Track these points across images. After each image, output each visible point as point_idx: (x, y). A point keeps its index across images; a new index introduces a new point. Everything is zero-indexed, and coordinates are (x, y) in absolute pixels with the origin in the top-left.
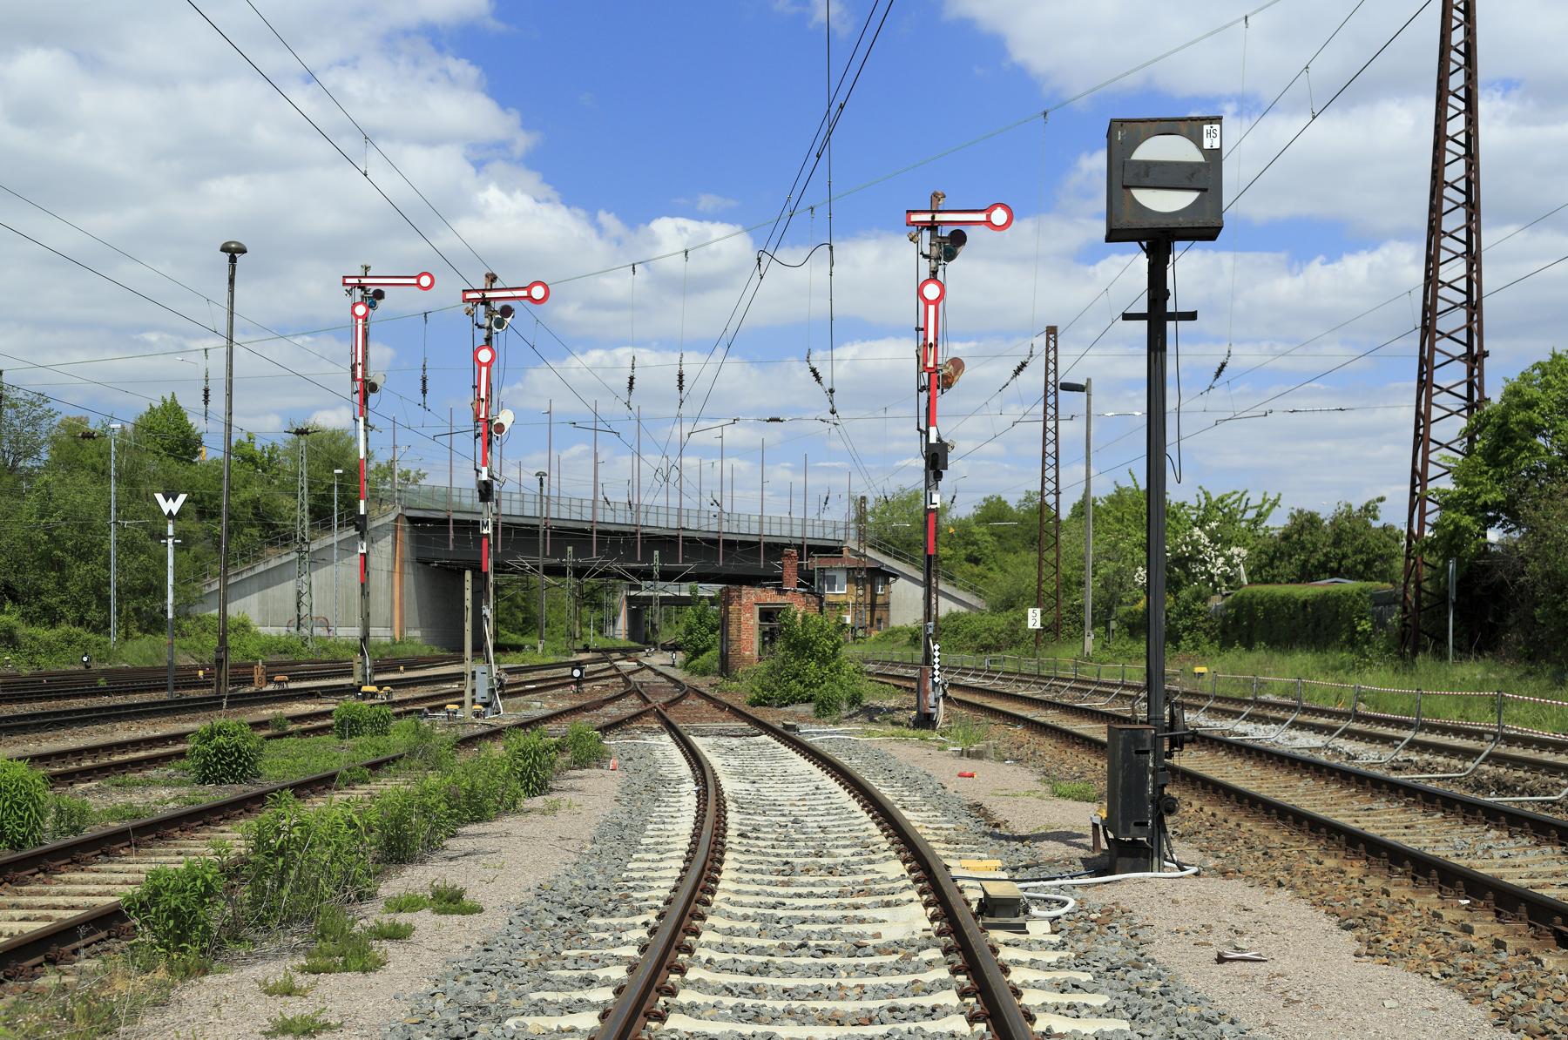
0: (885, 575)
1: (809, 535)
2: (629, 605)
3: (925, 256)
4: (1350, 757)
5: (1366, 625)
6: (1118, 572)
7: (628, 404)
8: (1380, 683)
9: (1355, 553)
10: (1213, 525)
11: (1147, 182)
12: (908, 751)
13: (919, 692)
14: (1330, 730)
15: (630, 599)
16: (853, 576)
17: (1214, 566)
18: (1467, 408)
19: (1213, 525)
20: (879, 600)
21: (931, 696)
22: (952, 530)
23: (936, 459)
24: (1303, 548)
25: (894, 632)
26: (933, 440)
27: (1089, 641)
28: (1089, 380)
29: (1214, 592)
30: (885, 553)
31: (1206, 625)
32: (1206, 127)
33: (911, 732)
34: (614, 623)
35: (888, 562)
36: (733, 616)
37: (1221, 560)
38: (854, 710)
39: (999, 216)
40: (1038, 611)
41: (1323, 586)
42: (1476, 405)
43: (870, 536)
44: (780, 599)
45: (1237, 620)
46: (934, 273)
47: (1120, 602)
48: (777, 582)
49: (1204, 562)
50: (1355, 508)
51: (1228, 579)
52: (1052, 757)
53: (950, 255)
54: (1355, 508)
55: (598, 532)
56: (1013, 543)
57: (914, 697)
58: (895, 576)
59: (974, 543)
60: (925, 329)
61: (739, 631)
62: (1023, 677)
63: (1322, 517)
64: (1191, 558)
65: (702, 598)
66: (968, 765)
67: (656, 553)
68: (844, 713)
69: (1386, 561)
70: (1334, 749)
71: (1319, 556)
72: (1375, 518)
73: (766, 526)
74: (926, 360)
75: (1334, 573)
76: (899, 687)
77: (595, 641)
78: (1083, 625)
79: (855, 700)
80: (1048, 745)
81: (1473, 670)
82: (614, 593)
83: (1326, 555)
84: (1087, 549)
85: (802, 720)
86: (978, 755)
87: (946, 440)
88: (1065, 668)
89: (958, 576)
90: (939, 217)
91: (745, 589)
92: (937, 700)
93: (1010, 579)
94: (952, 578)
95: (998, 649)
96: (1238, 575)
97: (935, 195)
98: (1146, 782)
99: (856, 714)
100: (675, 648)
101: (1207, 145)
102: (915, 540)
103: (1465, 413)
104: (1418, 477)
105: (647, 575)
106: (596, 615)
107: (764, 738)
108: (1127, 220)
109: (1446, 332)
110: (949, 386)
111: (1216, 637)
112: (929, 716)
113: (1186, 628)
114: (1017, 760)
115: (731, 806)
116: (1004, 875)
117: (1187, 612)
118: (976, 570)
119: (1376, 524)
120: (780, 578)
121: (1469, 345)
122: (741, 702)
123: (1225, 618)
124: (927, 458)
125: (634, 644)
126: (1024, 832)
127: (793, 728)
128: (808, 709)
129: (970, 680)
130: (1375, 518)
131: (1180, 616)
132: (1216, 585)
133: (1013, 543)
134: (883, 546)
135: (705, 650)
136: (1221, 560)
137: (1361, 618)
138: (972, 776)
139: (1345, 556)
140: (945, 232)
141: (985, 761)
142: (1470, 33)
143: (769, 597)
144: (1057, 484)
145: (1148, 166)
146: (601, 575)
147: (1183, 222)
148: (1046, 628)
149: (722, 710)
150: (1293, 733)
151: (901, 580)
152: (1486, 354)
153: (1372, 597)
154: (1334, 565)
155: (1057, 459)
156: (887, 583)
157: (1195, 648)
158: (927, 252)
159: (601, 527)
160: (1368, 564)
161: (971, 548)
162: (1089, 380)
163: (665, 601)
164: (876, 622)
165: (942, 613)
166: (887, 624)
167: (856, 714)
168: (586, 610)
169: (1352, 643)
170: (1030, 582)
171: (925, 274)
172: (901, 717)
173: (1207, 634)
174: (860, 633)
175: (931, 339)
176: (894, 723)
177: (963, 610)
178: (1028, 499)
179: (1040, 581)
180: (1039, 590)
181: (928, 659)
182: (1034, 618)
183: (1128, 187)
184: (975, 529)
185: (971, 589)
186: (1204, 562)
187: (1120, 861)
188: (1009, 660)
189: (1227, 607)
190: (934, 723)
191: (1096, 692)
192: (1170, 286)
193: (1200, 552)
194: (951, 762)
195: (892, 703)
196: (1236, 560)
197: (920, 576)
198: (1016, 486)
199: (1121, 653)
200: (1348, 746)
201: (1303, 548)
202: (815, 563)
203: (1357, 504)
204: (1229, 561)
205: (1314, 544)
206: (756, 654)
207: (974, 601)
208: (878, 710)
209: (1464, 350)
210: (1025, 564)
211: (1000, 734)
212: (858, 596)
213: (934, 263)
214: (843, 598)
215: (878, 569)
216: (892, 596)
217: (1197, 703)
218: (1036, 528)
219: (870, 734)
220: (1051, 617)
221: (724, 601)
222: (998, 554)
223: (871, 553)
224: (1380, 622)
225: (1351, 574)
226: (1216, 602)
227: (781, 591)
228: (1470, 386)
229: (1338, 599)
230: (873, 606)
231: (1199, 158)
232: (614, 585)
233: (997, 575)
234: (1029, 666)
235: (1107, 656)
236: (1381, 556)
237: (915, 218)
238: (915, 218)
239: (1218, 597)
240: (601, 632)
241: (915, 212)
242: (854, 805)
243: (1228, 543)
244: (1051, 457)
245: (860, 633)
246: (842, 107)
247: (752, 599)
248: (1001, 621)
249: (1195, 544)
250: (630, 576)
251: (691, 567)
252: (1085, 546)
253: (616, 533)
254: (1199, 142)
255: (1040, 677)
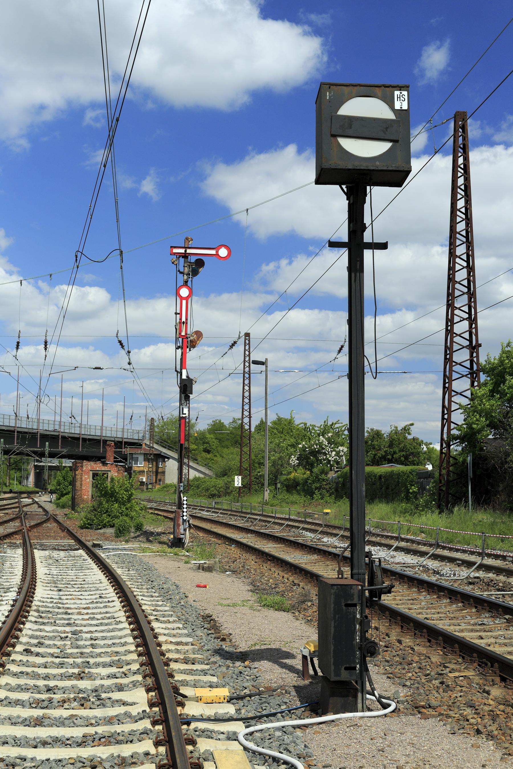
0: (164, 458)
1: (125, 437)
2: (35, 470)
3: (181, 273)
4: (436, 572)
5: (414, 489)
6: (280, 458)
7: (15, 357)
8: (432, 520)
9: (400, 451)
10: (330, 435)
11: (350, 132)
12: (167, 565)
13: (176, 526)
14: (422, 554)
15: (36, 467)
16: (147, 458)
17: (330, 456)
18: (470, 373)
19: (330, 435)
20: (160, 470)
21: (182, 527)
22: (196, 435)
23: (186, 388)
24: (374, 448)
25: (167, 486)
26: (184, 377)
27: (267, 494)
28: (266, 359)
29: (331, 470)
30: (163, 447)
31: (327, 487)
32: (397, 93)
33: (169, 550)
34: (27, 478)
35: (164, 451)
36: (78, 477)
37: (334, 453)
38: (138, 533)
39: (223, 252)
40: (240, 477)
41: (384, 469)
42: (474, 372)
43: (156, 438)
44: (104, 468)
45: (344, 484)
46: (186, 282)
47: (282, 474)
48: (101, 459)
49: (325, 454)
50: (399, 429)
51: (338, 463)
52: (255, 570)
53: (195, 273)
54: (399, 429)
55: (18, 432)
56: (226, 443)
57: (171, 524)
58: (168, 458)
59: (208, 443)
60: (180, 313)
61: (81, 485)
62: (233, 513)
63: (383, 432)
64: (319, 452)
65: (65, 467)
66: (203, 577)
67: (47, 443)
68: (132, 535)
69: (415, 456)
70: (424, 566)
71: (382, 453)
72: (409, 434)
73: (104, 432)
74: (181, 331)
75: (390, 461)
76: (166, 517)
77: (16, 487)
78: (263, 485)
79: (139, 527)
80: (251, 561)
81: (483, 516)
82: (28, 463)
83: (385, 452)
84: (265, 445)
85: (107, 539)
86: (209, 569)
87: (191, 377)
88: (255, 508)
89: (199, 459)
90: (189, 251)
91: (85, 463)
92: (185, 530)
93: (225, 461)
94: (196, 460)
95: (219, 496)
96: (342, 460)
97: (187, 239)
98: (354, 632)
99: (138, 536)
100: (52, 492)
101: (397, 106)
102: (181, 440)
103: (469, 376)
104: (446, 411)
105: (42, 455)
106: (18, 474)
107: (81, 552)
108: (335, 162)
109: (458, 337)
110: (194, 347)
111: (333, 493)
112: (180, 540)
113: (316, 488)
114: (234, 572)
115: (33, 616)
116: (230, 709)
117: (317, 479)
118: (209, 456)
119: (410, 437)
120: (104, 458)
121: (470, 340)
122: (73, 525)
123: (337, 483)
124: (180, 387)
125: (37, 489)
126: (243, 647)
127: (99, 546)
128: (110, 531)
129: (205, 514)
130: (409, 434)
131: (314, 482)
132: (332, 466)
133: (226, 443)
134: (162, 443)
135: (66, 494)
136: (334, 453)
137: (412, 485)
138: (205, 587)
139: (395, 453)
140: (193, 259)
141: (214, 574)
142: (467, 180)
143: (98, 466)
144: (250, 412)
145: (351, 120)
146: (17, 454)
147: (379, 165)
148: (244, 486)
149: (63, 531)
150: (395, 553)
151: (171, 460)
152: (480, 345)
153: (418, 474)
154: (390, 457)
155: (250, 399)
156: (165, 462)
157: (322, 498)
158: (182, 270)
159: (19, 430)
160: (406, 457)
161: (206, 445)
162: (266, 359)
163: (51, 468)
164: (158, 481)
165: (191, 477)
166: (164, 482)
167: (138, 536)
168: (12, 472)
169: (407, 499)
170: (235, 462)
171: (181, 283)
172: (164, 538)
173: (328, 491)
174: (150, 486)
175: (184, 319)
176: (160, 543)
177: (202, 476)
178: (234, 421)
179: (241, 462)
180: (241, 466)
181: (180, 505)
182: (238, 481)
183: (335, 136)
184: (208, 436)
185: (206, 465)
186: (325, 454)
187: (332, 700)
188: (225, 503)
189: (338, 477)
190: (184, 544)
191: (275, 523)
192: (367, 220)
193: (324, 449)
194: (192, 574)
195: (159, 530)
196: (342, 453)
197: (176, 456)
198: (229, 416)
199: (283, 500)
200: (433, 564)
201: (374, 448)
202: (127, 451)
203: (400, 426)
204: (338, 454)
205: (379, 446)
206: (90, 497)
207: (207, 472)
208: (152, 533)
209: (467, 343)
210: (232, 453)
211: (225, 552)
212: (149, 468)
213: (186, 277)
214: (142, 469)
215: (160, 454)
216: (167, 468)
217: (334, 532)
218: (237, 437)
219: (144, 550)
220: (246, 480)
221: (73, 469)
222: (219, 448)
223: (156, 446)
224: (422, 488)
225: (398, 462)
226: (332, 475)
227: (104, 464)
228: (472, 362)
229: (399, 475)
230: (157, 473)
231: (390, 115)
232: (28, 459)
233: (219, 459)
234: (236, 506)
235: (276, 502)
236: (412, 453)
237: (175, 251)
238: (175, 251)
239: (333, 472)
240: (20, 483)
241: (175, 247)
242: (122, 615)
243: (337, 445)
244: (247, 400)
245: (150, 486)
246: (117, 120)
247: (89, 467)
248: (221, 482)
249: (321, 444)
250: (33, 455)
251: (65, 451)
252: (262, 444)
253: (26, 433)
254: (391, 105)
255: (242, 512)
